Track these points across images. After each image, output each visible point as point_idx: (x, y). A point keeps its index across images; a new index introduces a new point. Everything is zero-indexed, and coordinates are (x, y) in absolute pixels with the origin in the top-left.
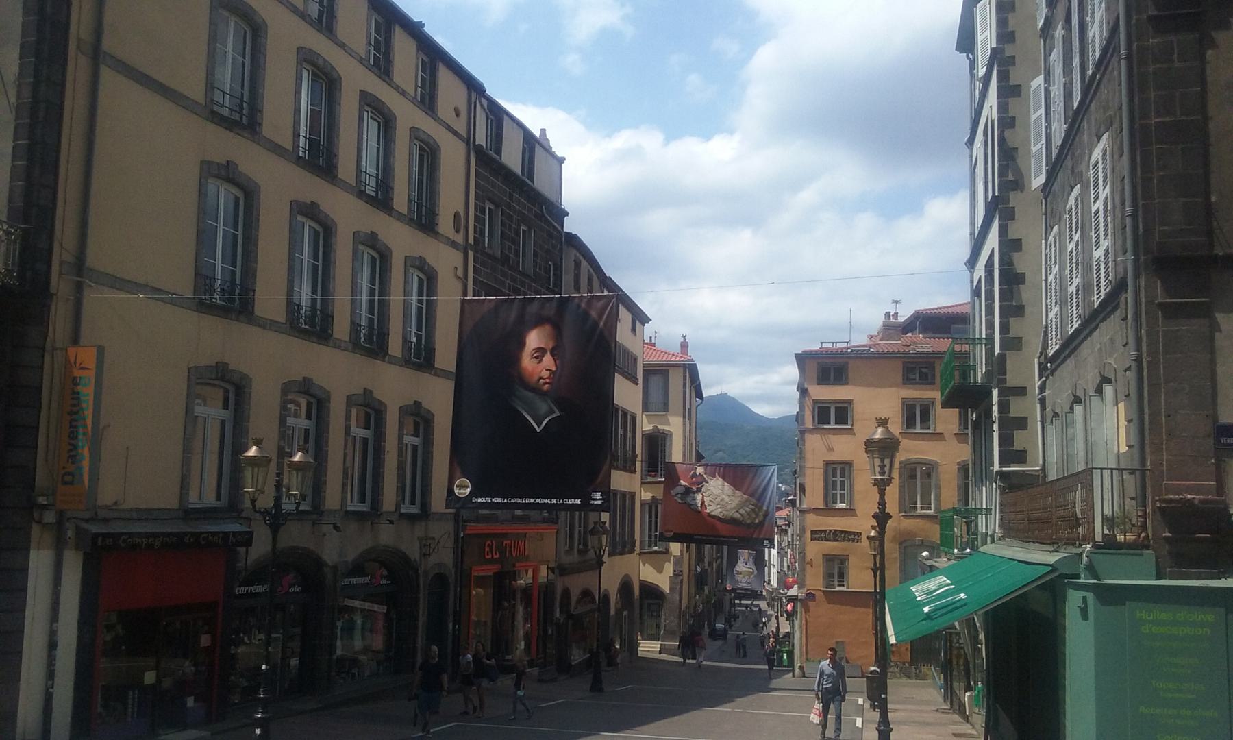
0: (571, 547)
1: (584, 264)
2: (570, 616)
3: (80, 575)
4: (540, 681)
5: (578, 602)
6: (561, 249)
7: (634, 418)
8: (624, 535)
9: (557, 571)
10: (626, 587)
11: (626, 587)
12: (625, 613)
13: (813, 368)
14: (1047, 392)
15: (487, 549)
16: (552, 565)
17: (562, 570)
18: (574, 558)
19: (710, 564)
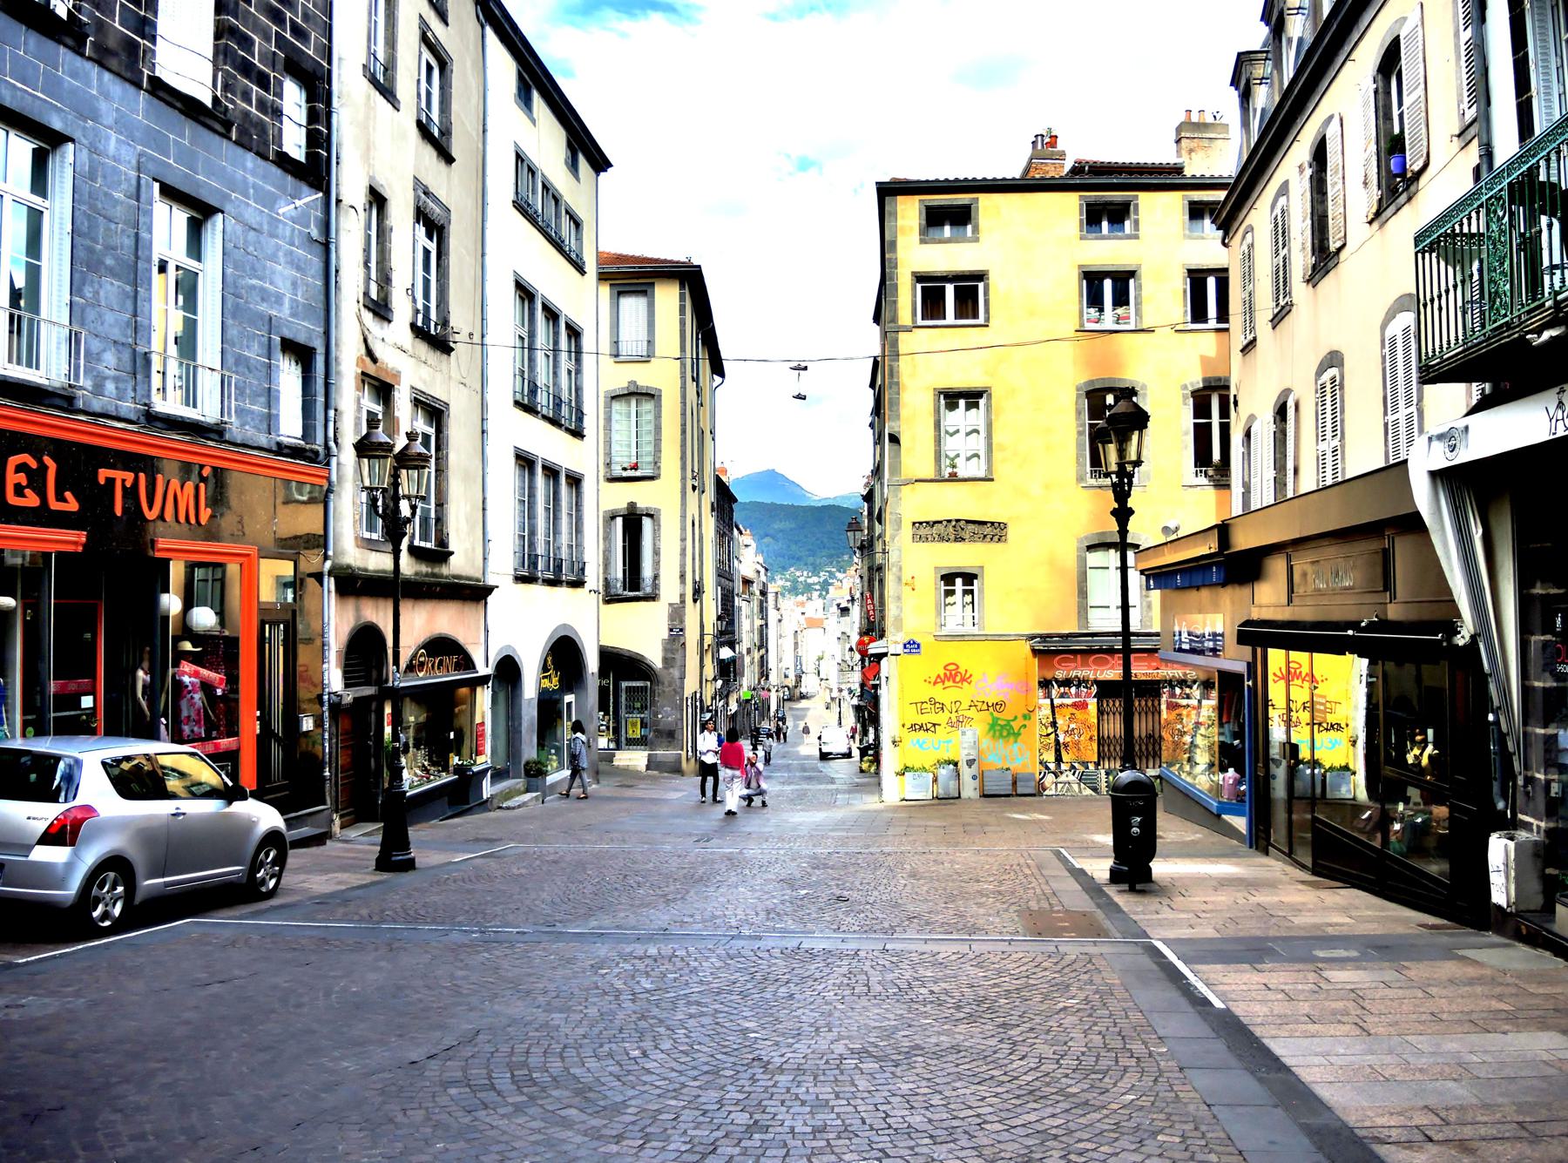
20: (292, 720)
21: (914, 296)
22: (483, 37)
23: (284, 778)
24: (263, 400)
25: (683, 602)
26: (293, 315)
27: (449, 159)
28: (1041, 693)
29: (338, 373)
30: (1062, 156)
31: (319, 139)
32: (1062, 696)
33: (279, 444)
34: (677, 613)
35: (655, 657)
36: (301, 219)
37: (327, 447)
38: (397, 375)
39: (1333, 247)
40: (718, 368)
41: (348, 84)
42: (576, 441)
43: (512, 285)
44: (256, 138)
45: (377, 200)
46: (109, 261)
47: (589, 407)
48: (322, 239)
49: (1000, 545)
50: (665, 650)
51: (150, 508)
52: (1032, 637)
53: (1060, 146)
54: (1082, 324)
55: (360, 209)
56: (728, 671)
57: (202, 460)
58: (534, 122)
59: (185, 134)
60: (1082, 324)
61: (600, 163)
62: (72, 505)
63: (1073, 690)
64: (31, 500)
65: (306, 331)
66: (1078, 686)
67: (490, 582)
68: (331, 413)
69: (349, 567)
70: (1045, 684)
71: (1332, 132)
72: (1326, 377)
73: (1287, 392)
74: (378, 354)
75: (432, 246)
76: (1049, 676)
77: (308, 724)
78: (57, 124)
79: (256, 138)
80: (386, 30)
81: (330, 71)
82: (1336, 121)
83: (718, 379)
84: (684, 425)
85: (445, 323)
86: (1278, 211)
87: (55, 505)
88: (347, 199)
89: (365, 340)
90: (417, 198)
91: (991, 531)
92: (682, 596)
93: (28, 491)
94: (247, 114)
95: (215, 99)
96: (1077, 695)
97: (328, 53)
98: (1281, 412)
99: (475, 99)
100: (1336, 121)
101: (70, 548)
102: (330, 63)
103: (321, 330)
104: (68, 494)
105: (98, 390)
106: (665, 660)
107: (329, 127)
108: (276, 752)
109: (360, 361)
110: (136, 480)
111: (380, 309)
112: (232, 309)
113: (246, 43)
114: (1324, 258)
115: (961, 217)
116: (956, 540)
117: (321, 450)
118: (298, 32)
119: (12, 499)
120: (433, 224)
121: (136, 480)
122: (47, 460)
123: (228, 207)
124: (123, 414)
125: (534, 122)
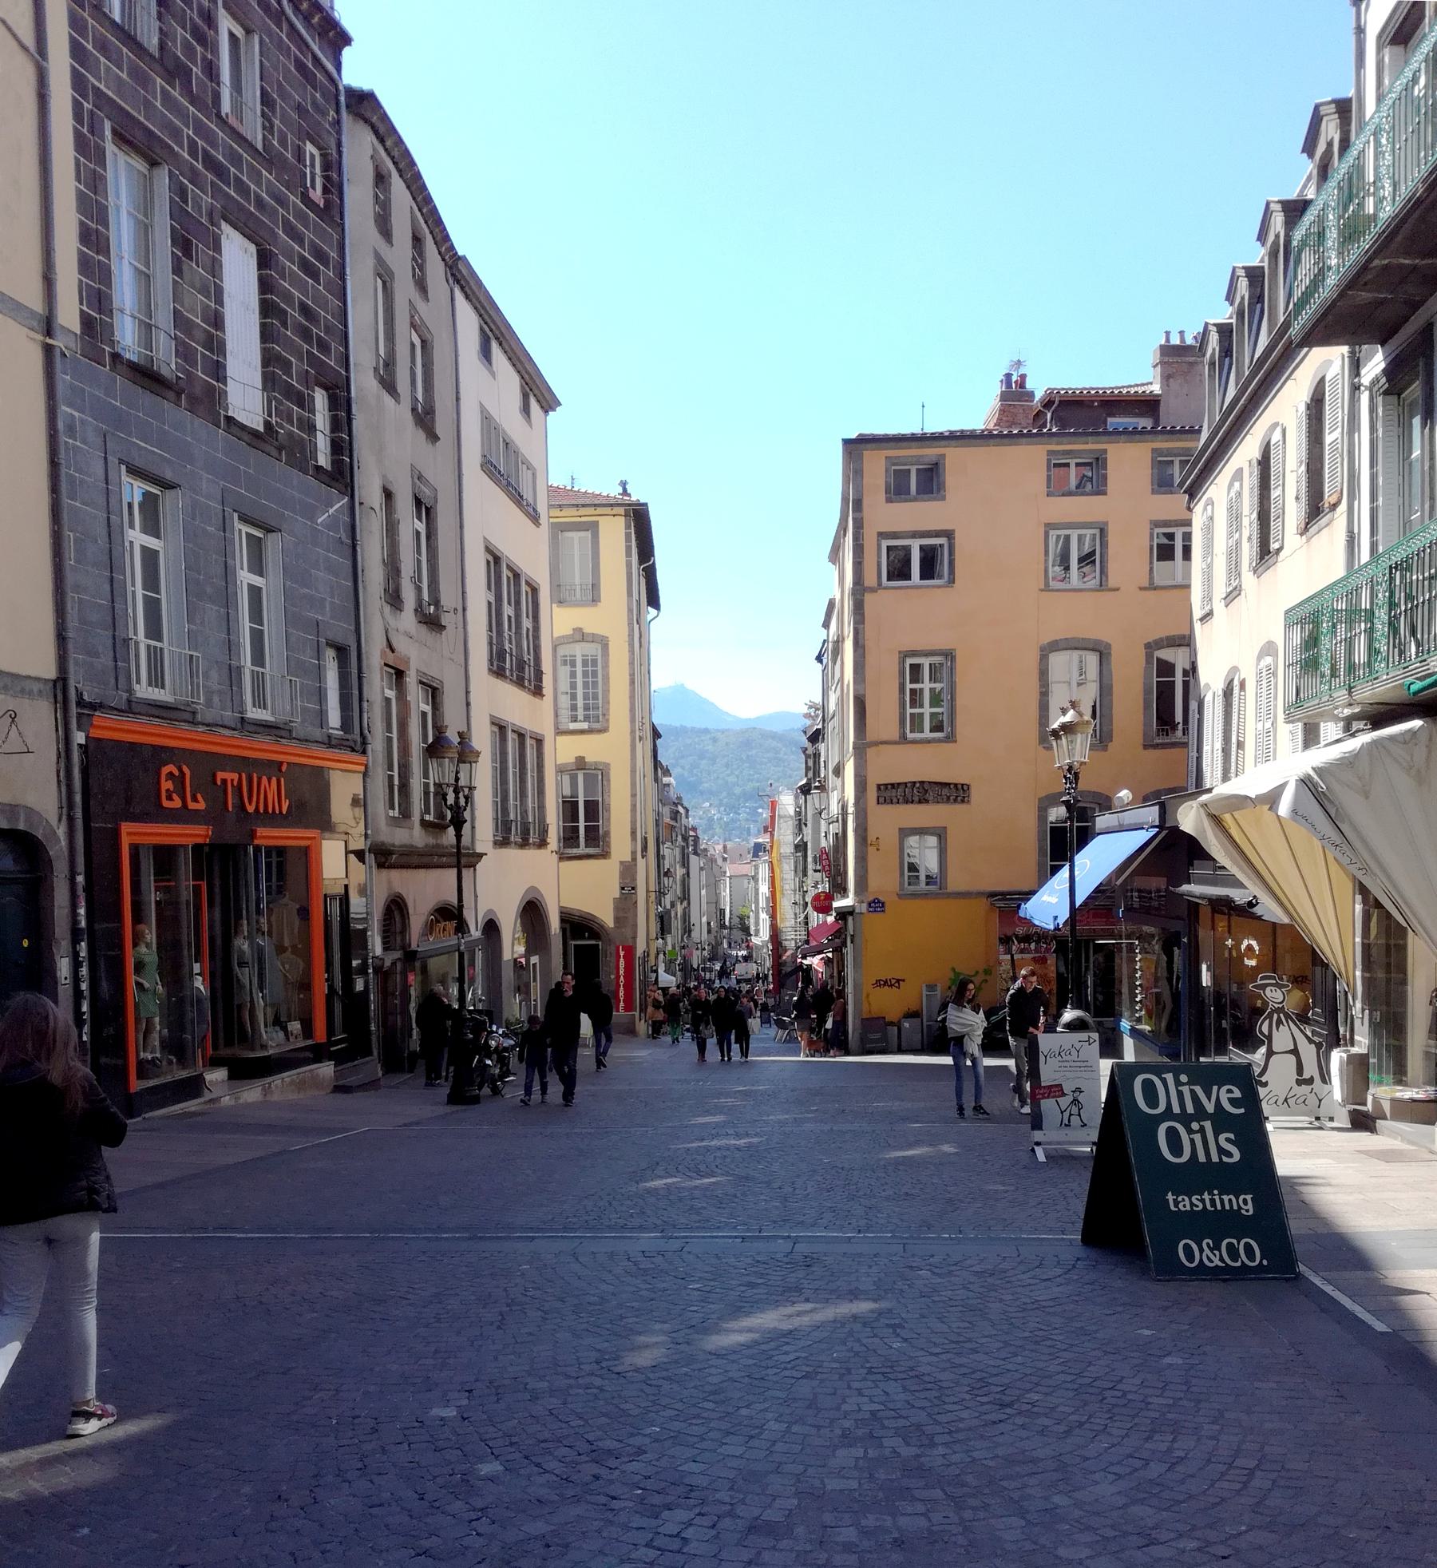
0: (406, 814)
1: (397, 185)
2: (410, 957)
3: (59, 1218)
4: (339, 1089)
5: (430, 927)
6: (338, 122)
7: (539, 742)
8: (524, 812)
9: (370, 858)
10: (532, 911)
11: (532, 911)
12: (534, 959)
13: (876, 465)
14: (778, 1056)
15: (167, 785)
16: (358, 844)
17: (383, 856)
18: (415, 836)
19: (673, 905)
20: (348, 983)
21: (879, 556)
22: (452, 299)
23: (344, 1032)
24: (316, 698)
25: (634, 859)
26: (332, 618)
27: (433, 437)
28: (1001, 949)
29: (368, 666)
30: (1031, 394)
31: (342, 447)
32: (1022, 951)
33: (329, 737)
34: (628, 870)
35: (607, 917)
36: (332, 524)
37: (362, 734)
38: (408, 662)
39: (1274, 546)
40: (653, 600)
41: (363, 382)
42: (536, 700)
43: (483, 549)
44: (299, 454)
45: (388, 495)
46: (209, 590)
47: (547, 666)
48: (349, 542)
49: (964, 806)
50: (617, 909)
51: (250, 803)
52: (992, 895)
53: (1029, 385)
54: (1047, 584)
55: (377, 509)
56: (664, 928)
57: (281, 758)
58: (493, 374)
59: (254, 461)
60: (1047, 584)
61: (549, 403)
62: (201, 805)
63: (1033, 946)
64: (177, 803)
65: (340, 630)
66: (1037, 942)
67: (479, 850)
68: (365, 704)
69: (383, 844)
70: (1006, 940)
71: (1276, 437)
72: (1263, 664)
73: (1235, 669)
74: (395, 645)
75: (421, 527)
76: (1009, 933)
77: (359, 985)
78: (168, 475)
79: (299, 454)
80: (385, 324)
81: (348, 379)
82: (1278, 430)
83: (652, 612)
84: (632, 675)
85: (436, 602)
86: (1233, 494)
87: (192, 805)
88: (368, 502)
89: (387, 632)
90: (414, 484)
91: (957, 793)
92: (634, 853)
93: (175, 796)
94: (290, 434)
95: (267, 424)
96: (1037, 950)
97: (346, 361)
98: (1228, 693)
99: (450, 371)
100: (1278, 430)
101: (200, 841)
102: (347, 370)
103: (352, 628)
104: (199, 796)
105: (209, 703)
106: (617, 919)
107: (350, 435)
108: (338, 1007)
109: (383, 653)
110: (240, 779)
111: (394, 599)
112: (292, 619)
113: (286, 366)
114: (1265, 552)
115: (931, 481)
116: (920, 802)
117: (359, 740)
118: (324, 347)
119: (166, 803)
120: (424, 508)
121: (240, 779)
122: (185, 769)
123: (284, 527)
124: (226, 723)
125: (493, 374)
